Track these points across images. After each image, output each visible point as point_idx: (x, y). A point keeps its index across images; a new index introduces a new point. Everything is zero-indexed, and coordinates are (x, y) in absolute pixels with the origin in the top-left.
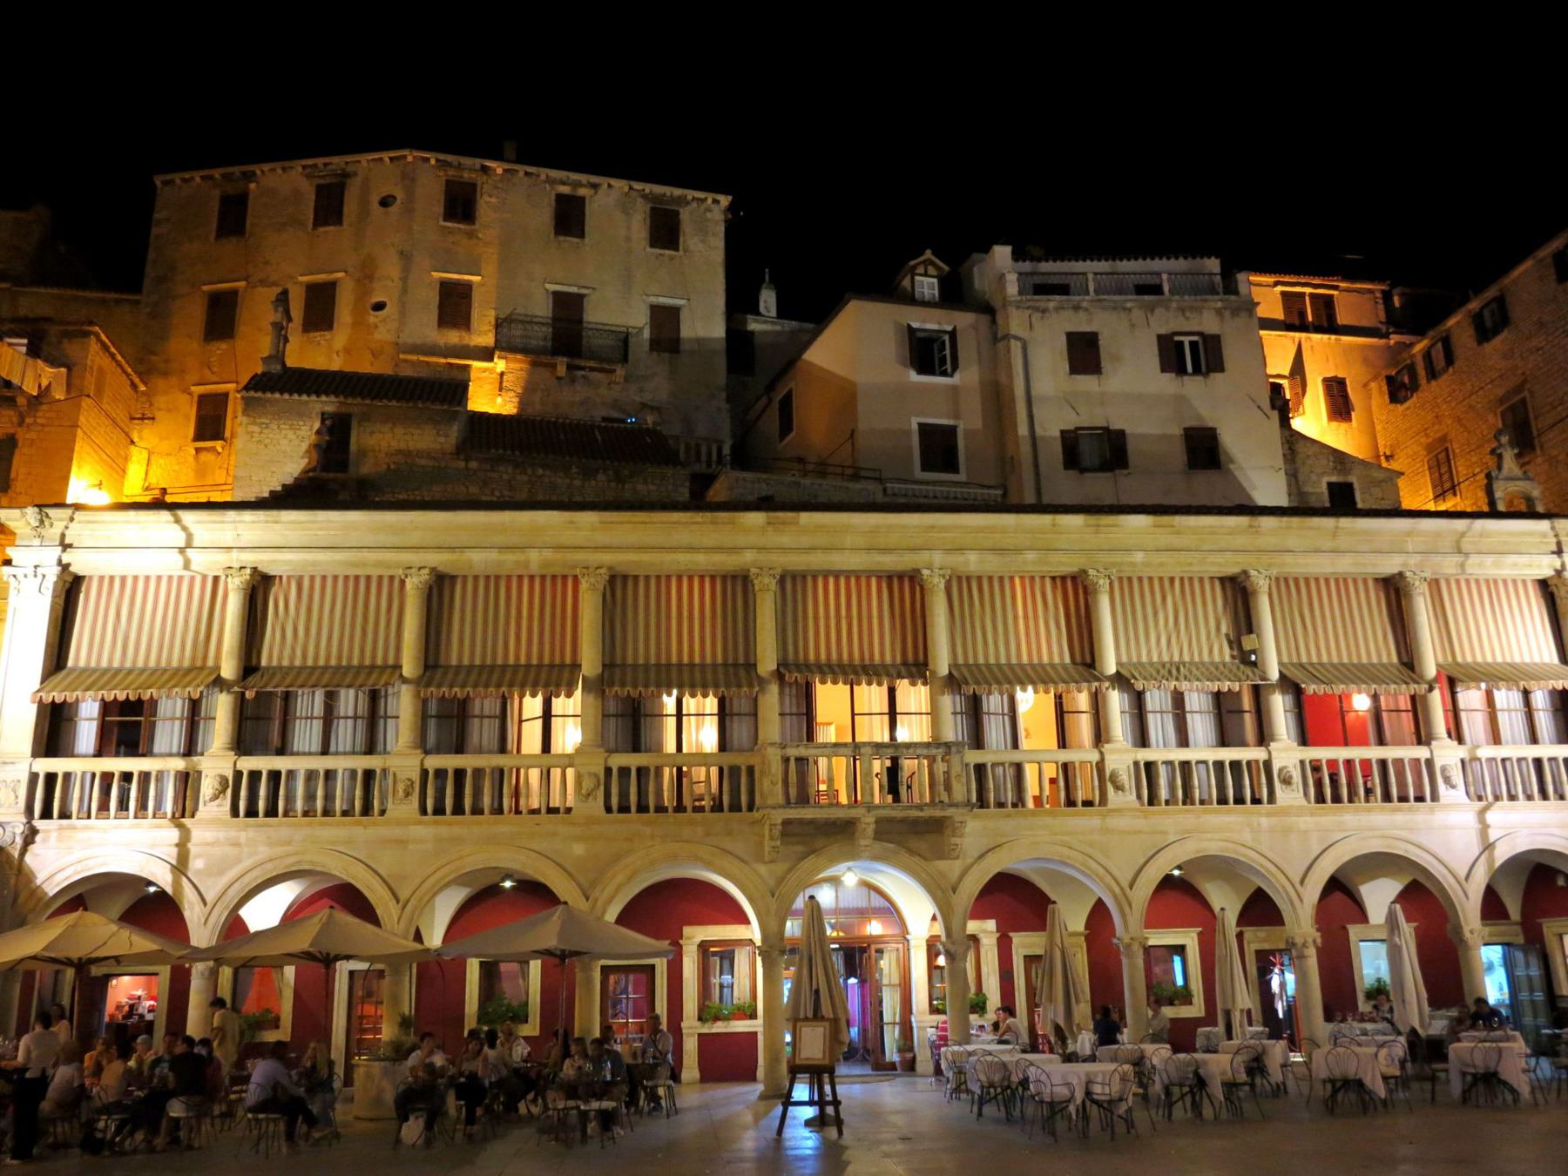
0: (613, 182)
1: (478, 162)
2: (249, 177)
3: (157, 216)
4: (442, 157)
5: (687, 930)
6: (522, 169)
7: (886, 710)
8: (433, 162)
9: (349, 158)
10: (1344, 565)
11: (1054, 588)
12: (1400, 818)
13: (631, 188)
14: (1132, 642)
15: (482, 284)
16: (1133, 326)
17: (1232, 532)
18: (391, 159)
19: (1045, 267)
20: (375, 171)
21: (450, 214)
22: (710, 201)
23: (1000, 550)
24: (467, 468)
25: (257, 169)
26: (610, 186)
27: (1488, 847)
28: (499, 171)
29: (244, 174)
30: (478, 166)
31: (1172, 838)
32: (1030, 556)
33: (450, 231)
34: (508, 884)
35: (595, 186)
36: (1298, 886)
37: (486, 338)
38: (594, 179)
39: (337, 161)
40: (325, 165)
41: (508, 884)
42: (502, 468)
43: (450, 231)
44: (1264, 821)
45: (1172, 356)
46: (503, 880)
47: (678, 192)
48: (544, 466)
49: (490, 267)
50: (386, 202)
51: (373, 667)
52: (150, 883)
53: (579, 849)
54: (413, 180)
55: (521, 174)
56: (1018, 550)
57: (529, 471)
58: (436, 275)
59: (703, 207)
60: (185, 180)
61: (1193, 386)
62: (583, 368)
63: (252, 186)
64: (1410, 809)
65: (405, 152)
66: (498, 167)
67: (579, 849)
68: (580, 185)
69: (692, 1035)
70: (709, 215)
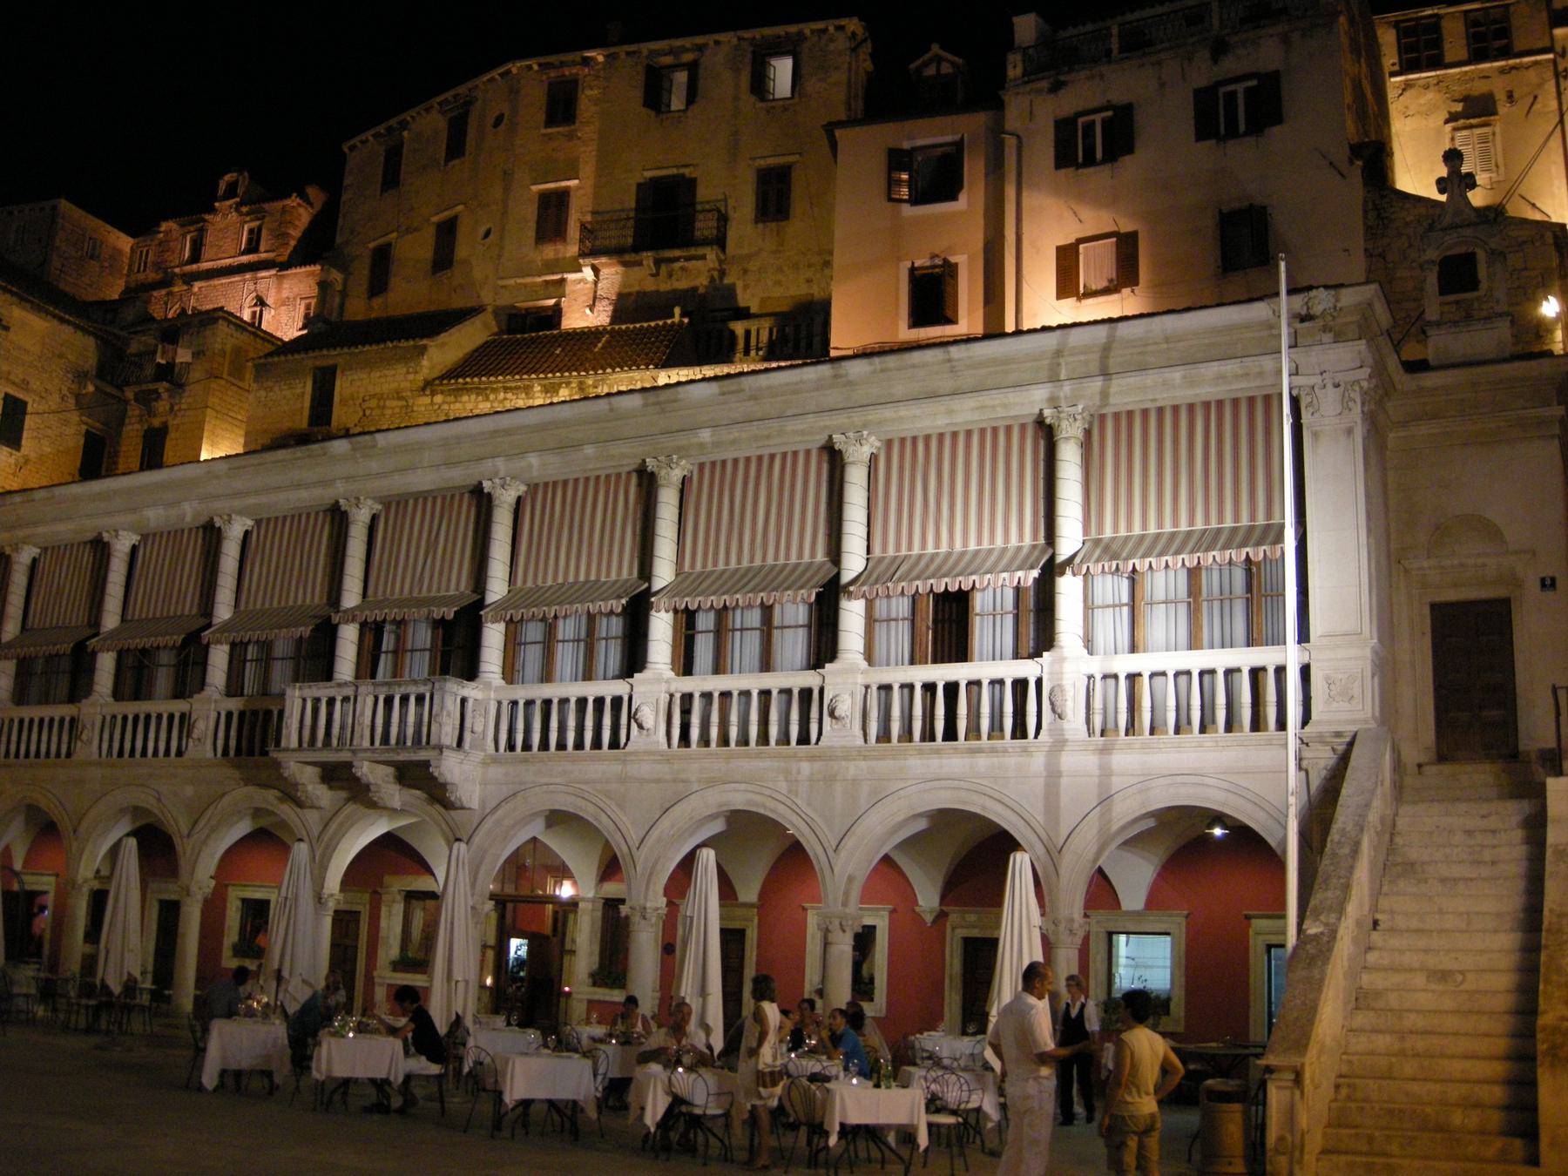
0: (722, 37)
1: (575, 56)
2: (404, 125)
3: (346, 182)
4: (542, 60)
5: (387, 879)
6: (622, 50)
7: (776, 633)
8: (536, 67)
9: (469, 85)
10: (966, 412)
11: (640, 485)
12: (982, 762)
13: (740, 39)
14: (574, 550)
15: (578, 188)
16: (1162, 85)
17: (819, 386)
18: (628, 54)
19: (1130, 17)
20: (488, 88)
21: (551, 121)
22: (831, 29)
23: (561, 448)
24: (432, 403)
25: (406, 116)
26: (717, 43)
27: (1105, 800)
28: (601, 59)
29: (400, 123)
30: (578, 59)
31: (695, 787)
32: (589, 450)
33: (550, 138)
34: (1218, 832)
35: (700, 48)
36: (634, 850)
37: (572, 249)
38: (699, 40)
39: (462, 90)
40: (455, 96)
41: (1218, 832)
42: (465, 398)
43: (550, 138)
44: (805, 767)
45: (1213, 118)
46: (1211, 826)
47: (793, 29)
48: (506, 389)
49: (588, 168)
50: (498, 121)
51: (57, 627)
52: (1218, 818)
53: (189, 790)
54: (518, 92)
55: (623, 56)
56: (578, 445)
57: (492, 397)
58: (535, 188)
59: (825, 37)
60: (362, 142)
61: (1241, 154)
62: (677, 259)
63: (405, 134)
64: (938, 752)
65: (510, 65)
66: (598, 56)
67: (189, 790)
68: (685, 50)
69: (381, 985)
70: (832, 47)
